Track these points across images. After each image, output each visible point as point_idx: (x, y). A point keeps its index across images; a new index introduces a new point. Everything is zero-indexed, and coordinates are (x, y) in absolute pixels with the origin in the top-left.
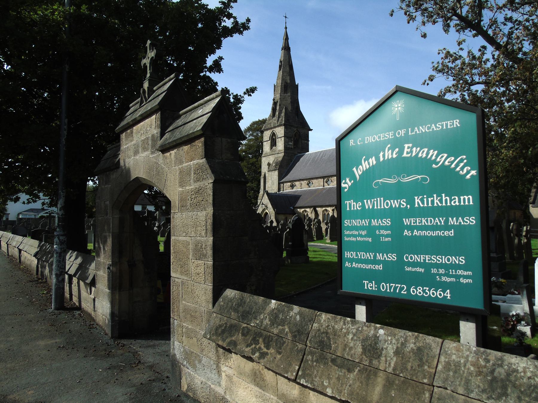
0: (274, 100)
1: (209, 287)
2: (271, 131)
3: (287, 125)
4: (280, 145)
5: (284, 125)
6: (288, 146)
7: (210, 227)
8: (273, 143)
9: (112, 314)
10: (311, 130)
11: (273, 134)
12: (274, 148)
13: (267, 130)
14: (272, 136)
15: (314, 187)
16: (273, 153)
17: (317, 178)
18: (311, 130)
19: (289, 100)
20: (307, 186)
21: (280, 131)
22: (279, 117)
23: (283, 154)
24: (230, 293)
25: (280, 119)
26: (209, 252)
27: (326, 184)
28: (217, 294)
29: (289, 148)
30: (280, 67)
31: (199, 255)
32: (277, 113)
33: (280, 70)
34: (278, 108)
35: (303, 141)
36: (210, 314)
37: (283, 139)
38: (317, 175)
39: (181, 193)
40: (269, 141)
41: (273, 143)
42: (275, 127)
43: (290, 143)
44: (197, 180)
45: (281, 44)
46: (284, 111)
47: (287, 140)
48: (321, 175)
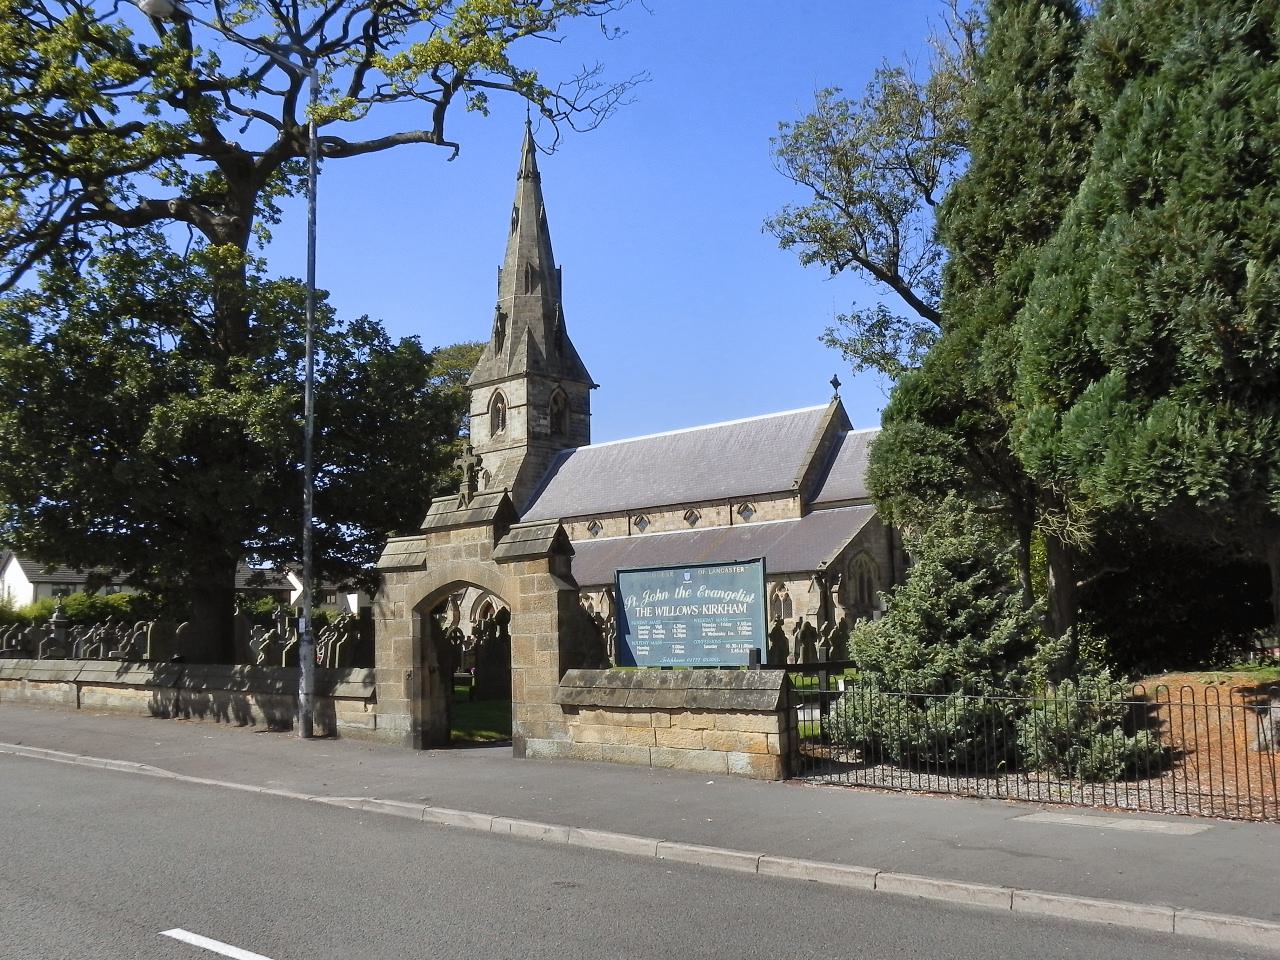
0: (499, 308)
1: (556, 669)
2: (493, 388)
3: (535, 374)
4: (517, 426)
5: (527, 375)
6: (538, 429)
7: (555, 625)
8: (498, 419)
9: (414, 725)
10: (596, 387)
11: (499, 398)
12: (499, 432)
13: (481, 385)
14: (496, 403)
15: (605, 535)
16: (499, 446)
17: (611, 515)
18: (596, 387)
19: (539, 311)
20: (588, 533)
21: (516, 392)
22: (512, 354)
23: (523, 451)
24: (573, 673)
25: (515, 359)
26: (556, 643)
27: (635, 529)
28: (562, 673)
29: (540, 433)
30: (515, 222)
31: (544, 645)
32: (507, 343)
33: (514, 230)
34: (509, 331)
35: (576, 416)
36: (555, 690)
37: (524, 410)
38: (612, 506)
39: (523, 599)
40: (488, 416)
41: (498, 419)
42: (503, 380)
43: (542, 422)
44: (540, 590)
45: (518, 161)
46: (525, 337)
47: (535, 413)
48: (623, 505)
